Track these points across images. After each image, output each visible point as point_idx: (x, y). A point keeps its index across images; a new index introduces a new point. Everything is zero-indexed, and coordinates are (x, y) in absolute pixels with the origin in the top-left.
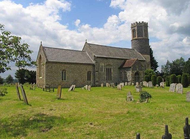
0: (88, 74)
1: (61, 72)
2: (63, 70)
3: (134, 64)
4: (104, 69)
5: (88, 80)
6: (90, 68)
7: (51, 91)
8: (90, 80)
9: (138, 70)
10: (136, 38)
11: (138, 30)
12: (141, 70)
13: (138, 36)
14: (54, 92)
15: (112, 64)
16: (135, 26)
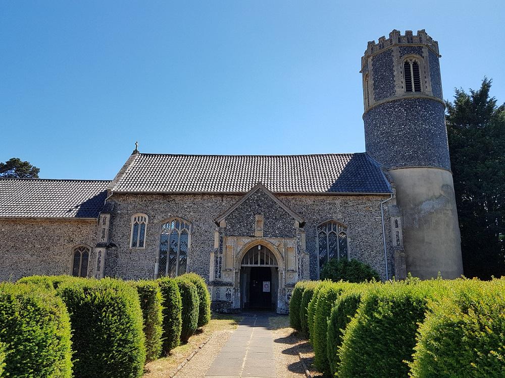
0: (77, 255)
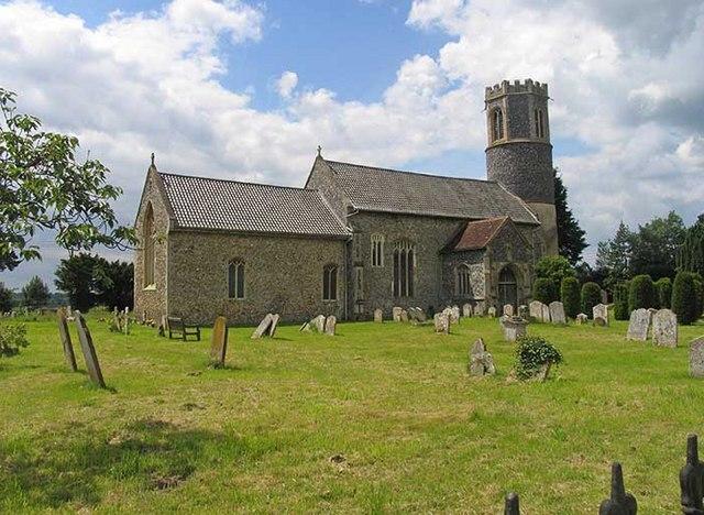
0: (326, 273)
1: (227, 266)
2: (235, 260)
3: (498, 237)
4: (386, 255)
5: (326, 297)
6: (334, 254)
7: (187, 337)
8: (334, 297)
9: (510, 258)
10: (505, 139)
11: (511, 111)
12: (523, 259)
13: (513, 135)
14: (199, 339)
15: (414, 237)
16: (502, 97)
